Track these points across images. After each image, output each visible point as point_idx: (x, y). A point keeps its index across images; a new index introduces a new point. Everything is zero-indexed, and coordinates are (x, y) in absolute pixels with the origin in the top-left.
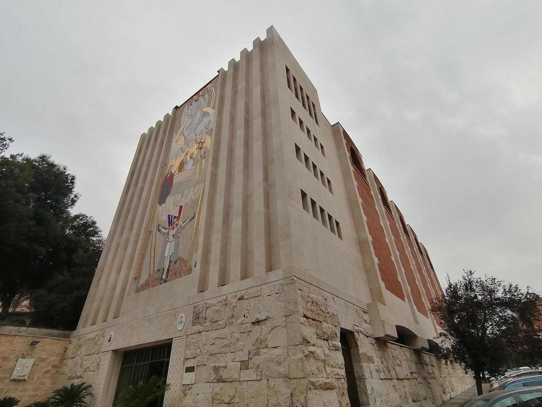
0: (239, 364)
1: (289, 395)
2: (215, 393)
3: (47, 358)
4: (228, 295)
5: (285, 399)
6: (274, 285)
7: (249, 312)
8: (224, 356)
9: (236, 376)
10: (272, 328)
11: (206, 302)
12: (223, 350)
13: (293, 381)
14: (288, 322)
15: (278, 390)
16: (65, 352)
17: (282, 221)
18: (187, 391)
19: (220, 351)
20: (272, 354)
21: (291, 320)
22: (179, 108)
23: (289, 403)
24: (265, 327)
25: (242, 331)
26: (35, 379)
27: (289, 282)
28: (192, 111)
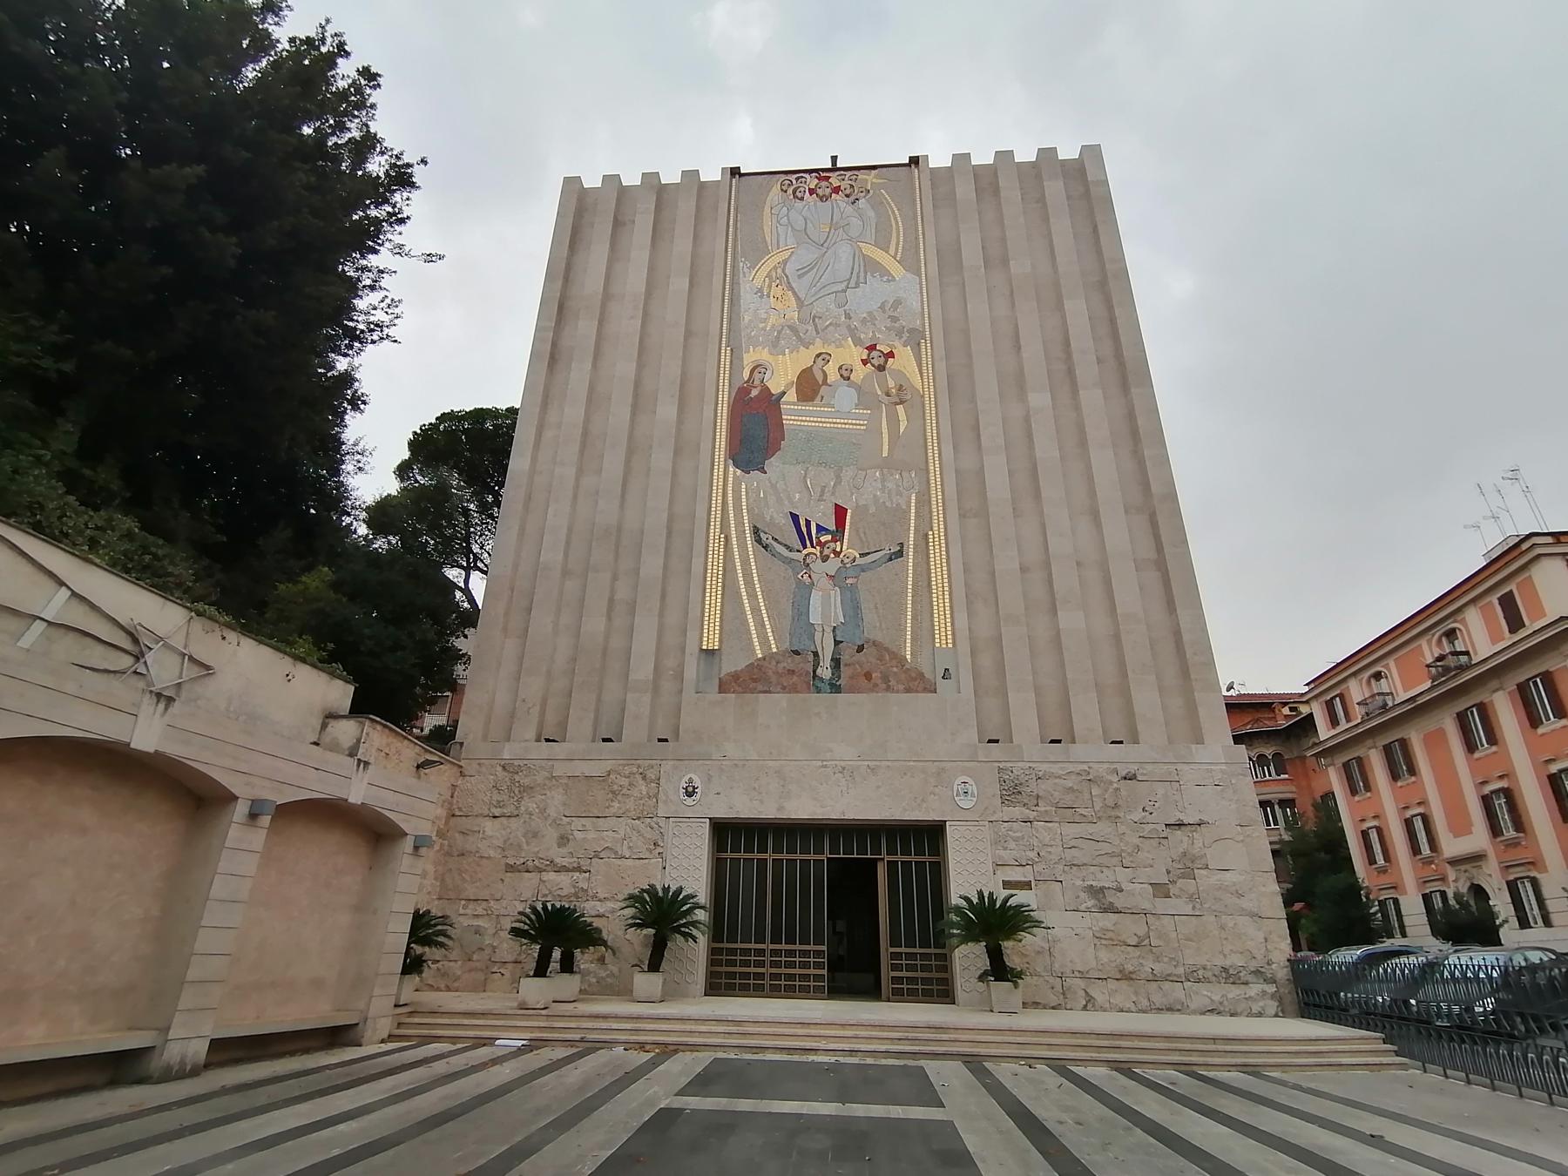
9: (1146, 905)
12: (1105, 860)
17: (1195, 654)
19: (1094, 863)
24: (1199, 837)
25: (485, 903)
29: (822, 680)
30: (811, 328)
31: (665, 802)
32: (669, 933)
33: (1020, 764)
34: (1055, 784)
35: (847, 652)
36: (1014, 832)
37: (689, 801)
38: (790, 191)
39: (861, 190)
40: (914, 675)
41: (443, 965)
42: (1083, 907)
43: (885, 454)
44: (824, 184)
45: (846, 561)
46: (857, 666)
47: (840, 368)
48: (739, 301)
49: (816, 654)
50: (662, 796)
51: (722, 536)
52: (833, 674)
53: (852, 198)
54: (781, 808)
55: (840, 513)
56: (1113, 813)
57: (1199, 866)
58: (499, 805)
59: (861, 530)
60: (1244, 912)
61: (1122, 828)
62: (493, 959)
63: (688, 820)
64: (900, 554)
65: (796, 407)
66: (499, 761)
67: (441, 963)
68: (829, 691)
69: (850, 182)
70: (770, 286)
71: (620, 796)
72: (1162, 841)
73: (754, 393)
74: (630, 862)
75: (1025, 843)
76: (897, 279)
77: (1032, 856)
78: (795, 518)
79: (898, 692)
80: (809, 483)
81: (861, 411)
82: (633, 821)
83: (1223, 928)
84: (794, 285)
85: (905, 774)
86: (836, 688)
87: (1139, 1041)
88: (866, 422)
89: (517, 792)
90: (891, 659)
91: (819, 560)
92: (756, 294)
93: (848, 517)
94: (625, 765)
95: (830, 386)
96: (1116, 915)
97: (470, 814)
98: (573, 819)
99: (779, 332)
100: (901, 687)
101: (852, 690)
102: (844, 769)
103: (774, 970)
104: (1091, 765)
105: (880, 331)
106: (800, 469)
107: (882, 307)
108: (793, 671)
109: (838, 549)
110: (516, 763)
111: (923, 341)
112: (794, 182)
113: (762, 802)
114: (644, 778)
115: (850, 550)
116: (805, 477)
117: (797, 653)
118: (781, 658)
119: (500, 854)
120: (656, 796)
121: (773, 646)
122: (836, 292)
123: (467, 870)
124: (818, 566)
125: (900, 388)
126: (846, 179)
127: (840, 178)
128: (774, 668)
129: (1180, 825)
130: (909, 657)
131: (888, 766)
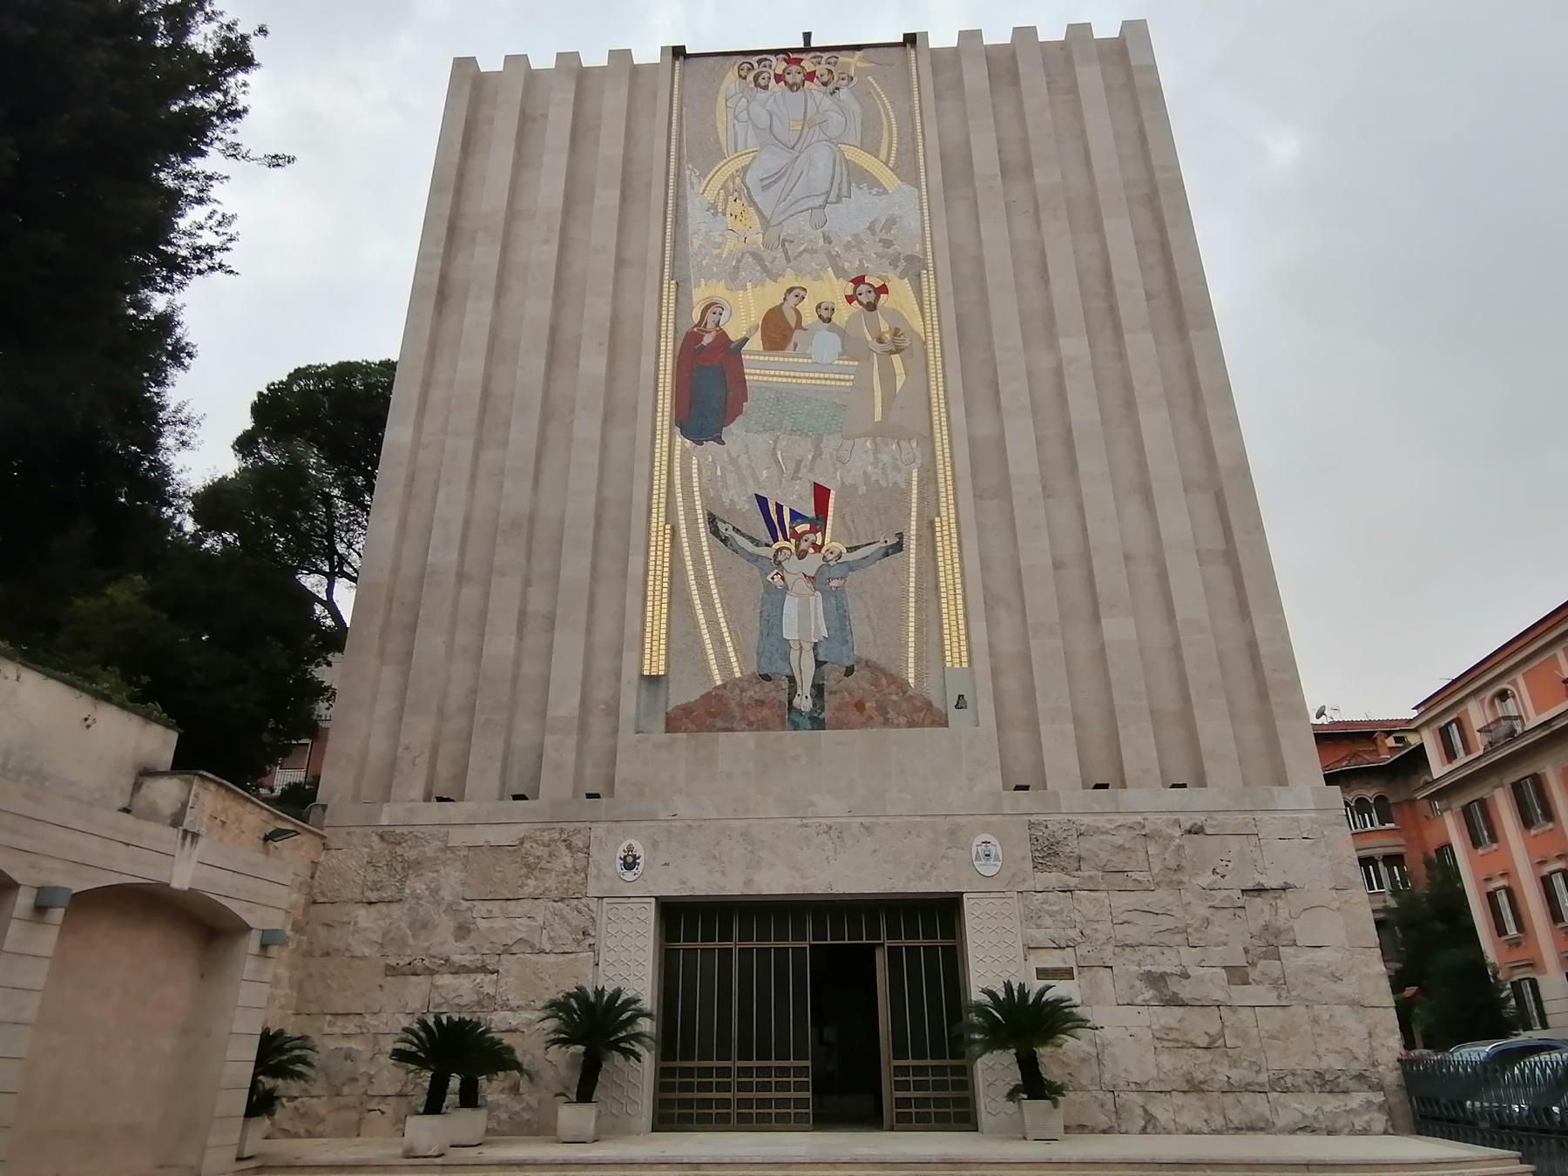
1: (1366, 1036)
2: (409, 928)
9: (1219, 995)
11: (1073, 818)
12: (1166, 938)
19: (1154, 941)
21: (1351, 898)
22: (687, 56)
23: (1367, 1048)
25: (1216, 903)
28: (774, 118)
29: (800, 712)
30: (779, 254)
31: (597, 878)
33: (1059, 817)
34: (1101, 841)
35: (831, 676)
36: (1051, 905)
37: (629, 876)
38: (750, 77)
39: (841, 76)
40: (919, 704)
41: (302, 1102)
42: (1139, 1000)
43: (878, 418)
44: (794, 68)
45: (830, 557)
47: (819, 306)
49: (792, 679)
50: (592, 870)
53: (831, 87)
54: (749, 882)
55: (821, 494)
57: (1285, 943)
59: (848, 518)
61: (1187, 896)
62: (369, 1093)
64: (899, 547)
65: (762, 358)
68: (810, 727)
70: (726, 201)
72: (1239, 912)
73: (707, 339)
74: (551, 958)
76: (890, 191)
78: (762, 502)
79: (898, 726)
81: (846, 363)
84: (757, 199)
86: (818, 723)
88: (852, 377)
90: (889, 684)
91: (795, 557)
92: (707, 211)
95: (806, 330)
97: (337, 900)
98: (475, 903)
100: (902, 720)
101: (840, 725)
102: (830, 828)
105: (869, 260)
106: (768, 438)
107: (871, 228)
109: (819, 542)
112: (756, 65)
114: (569, 847)
117: (767, 678)
120: (585, 869)
124: (792, 565)
125: (896, 333)
127: (814, 60)
129: (1260, 890)
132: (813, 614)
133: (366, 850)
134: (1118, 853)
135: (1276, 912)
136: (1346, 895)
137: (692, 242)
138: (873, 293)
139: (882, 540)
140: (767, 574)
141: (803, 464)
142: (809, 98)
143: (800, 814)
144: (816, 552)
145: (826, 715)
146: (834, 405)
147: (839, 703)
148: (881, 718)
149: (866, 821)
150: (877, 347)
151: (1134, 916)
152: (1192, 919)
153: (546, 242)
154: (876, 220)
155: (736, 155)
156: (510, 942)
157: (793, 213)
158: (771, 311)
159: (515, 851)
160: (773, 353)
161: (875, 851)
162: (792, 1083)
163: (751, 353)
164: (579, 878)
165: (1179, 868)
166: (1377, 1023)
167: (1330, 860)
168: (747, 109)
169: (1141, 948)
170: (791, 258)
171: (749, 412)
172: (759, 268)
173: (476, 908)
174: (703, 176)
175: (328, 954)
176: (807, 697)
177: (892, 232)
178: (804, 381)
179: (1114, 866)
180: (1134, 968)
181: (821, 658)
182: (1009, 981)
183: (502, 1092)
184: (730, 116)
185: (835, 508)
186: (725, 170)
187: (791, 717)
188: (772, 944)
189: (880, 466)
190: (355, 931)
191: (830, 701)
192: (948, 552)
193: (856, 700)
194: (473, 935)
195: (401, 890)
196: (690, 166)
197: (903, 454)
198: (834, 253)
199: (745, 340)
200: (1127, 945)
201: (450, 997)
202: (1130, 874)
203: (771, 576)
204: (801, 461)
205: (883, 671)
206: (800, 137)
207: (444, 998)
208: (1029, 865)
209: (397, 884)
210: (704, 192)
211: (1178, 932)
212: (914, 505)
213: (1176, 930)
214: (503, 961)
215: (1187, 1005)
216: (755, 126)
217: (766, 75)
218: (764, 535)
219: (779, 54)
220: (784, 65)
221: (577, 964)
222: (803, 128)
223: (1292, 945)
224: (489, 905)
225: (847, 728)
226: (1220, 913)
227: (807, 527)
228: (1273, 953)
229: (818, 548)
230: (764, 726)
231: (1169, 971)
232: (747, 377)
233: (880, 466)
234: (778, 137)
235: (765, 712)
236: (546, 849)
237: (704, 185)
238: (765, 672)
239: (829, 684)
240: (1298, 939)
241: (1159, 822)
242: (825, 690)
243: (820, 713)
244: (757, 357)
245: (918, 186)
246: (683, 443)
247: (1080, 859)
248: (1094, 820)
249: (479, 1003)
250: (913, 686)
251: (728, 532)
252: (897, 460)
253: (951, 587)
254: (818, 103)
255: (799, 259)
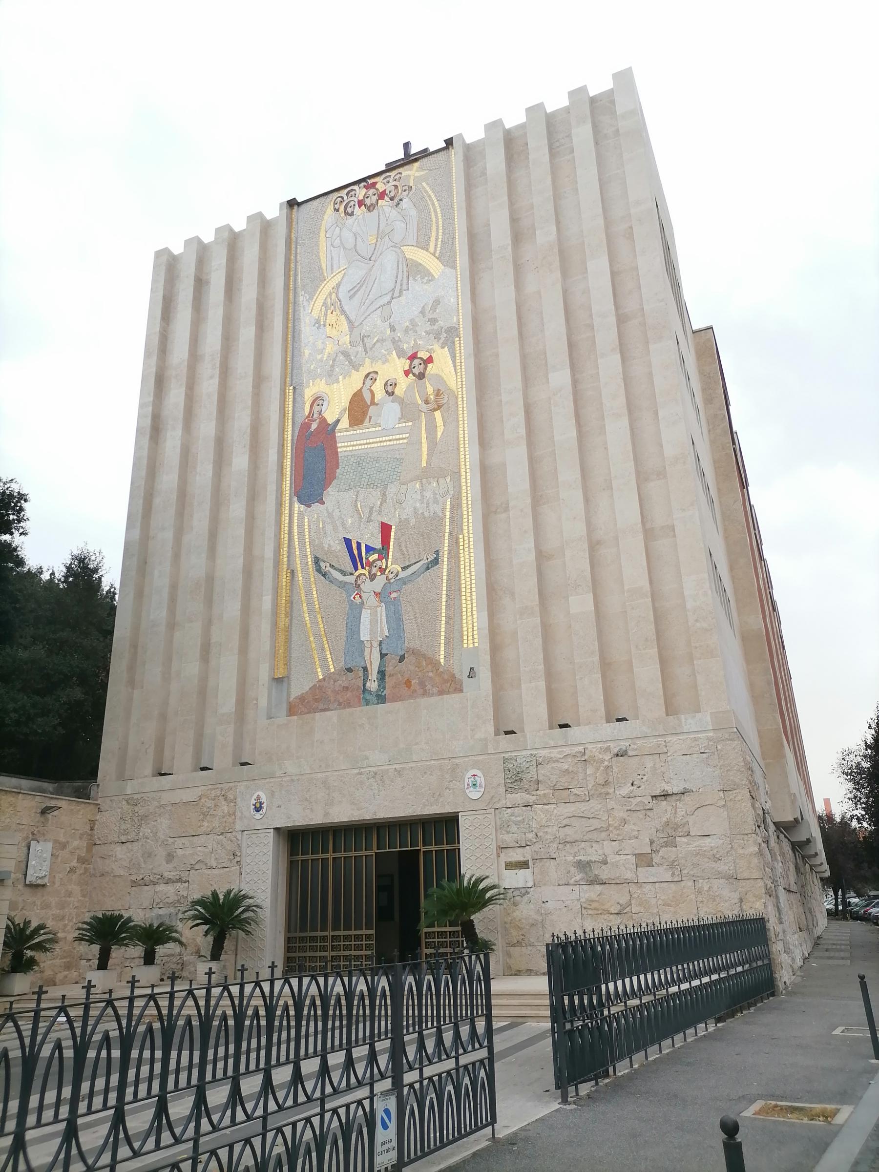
0: (633, 859)
1: (736, 901)
3: (68, 842)
4: (587, 746)
5: (731, 906)
6: (696, 739)
7: (642, 778)
8: (594, 845)
9: (629, 875)
10: (697, 806)
11: (534, 752)
12: (594, 836)
13: (742, 883)
14: (727, 799)
15: (717, 894)
16: (92, 829)
17: (697, 621)
18: (518, 898)
19: (585, 838)
20: (700, 846)
22: (299, 204)
24: (683, 807)
25: (633, 807)
26: (56, 886)
27: (727, 736)
28: (359, 239)
29: (370, 692)
30: (360, 349)
31: (241, 818)
32: (455, 885)
33: (524, 753)
34: (552, 768)
35: (390, 664)
36: (516, 817)
37: (258, 816)
38: (342, 209)
39: (404, 188)
40: (446, 677)
41: (93, 963)
42: (572, 882)
43: (424, 464)
44: (372, 191)
45: (391, 576)
46: (399, 675)
47: (386, 384)
48: (299, 335)
49: (365, 669)
50: (238, 814)
51: (289, 571)
52: (379, 686)
53: (396, 200)
54: (327, 814)
55: (385, 529)
56: (603, 790)
57: (681, 834)
58: (126, 832)
59: (403, 545)
60: (720, 875)
61: (611, 804)
62: (125, 956)
63: (257, 832)
64: (436, 561)
65: (348, 433)
66: (123, 797)
67: (92, 961)
68: (376, 702)
69: (394, 183)
70: (326, 315)
71: (208, 816)
72: (648, 813)
73: (314, 426)
74: (216, 871)
75: (525, 826)
76: (436, 277)
77: (530, 837)
78: (348, 542)
79: (433, 695)
80: (359, 506)
81: (404, 424)
82: (218, 837)
83: (699, 892)
84: (346, 308)
85: (425, 773)
86: (381, 699)
87: (539, 1014)
88: (408, 435)
89: (136, 821)
90: (427, 665)
91: (368, 580)
92: (314, 326)
93: (393, 534)
94: (212, 790)
95: (377, 404)
96: (603, 886)
97: (106, 842)
98: (175, 839)
99: (334, 360)
100: (435, 690)
101: (396, 699)
102: (376, 774)
103: (334, 953)
104: (587, 746)
105: (421, 338)
106: (352, 494)
107: (422, 312)
108: (347, 688)
109: (384, 567)
110: (135, 797)
111: (457, 339)
112: (345, 197)
113: (312, 810)
114: (225, 800)
115: (394, 566)
116: (356, 501)
117: (350, 670)
118: (337, 676)
119: (127, 872)
120: (234, 814)
121: (331, 667)
122: (382, 306)
123: (105, 887)
124: (368, 587)
125: (438, 393)
126: (391, 180)
127: (385, 181)
128: (332, 687)
129: (665, 796)
130: (442, 660)
131: (412, 768)
132: (379, 620)
133: (119, 810)
134: (564, 775)
135: (676, 811)
136: (731, 795)
137: (304, 352)
138: (423, 364)
139: (425, 558)
140: (351, 595)
141: (374, 509)
142: (381, 214)
143: (359, 765)
144: (382, 574)
145: (387, 692)
146: (395, 460)
147: (395, 683)
148: (422, 690)
149: (397, 766)
150: (424, 407)
151: (574, 822)
152: (614, 820)
153: (211, 377)
154: (426, 304)
155: (332, 276)
156: (194, 863)
157: (369, 313)
158: (355, 395)
159: (197, 805)
160: (356, 428)
161: (403, 787)
162: (353, 945)
163: (342, 431)
164: (230, 820)
165: (607, 783)
166: (747, 891)
167: (721, 769)
168: (340, 236)
169: (576, 844)
170: (368, 350)
171: (340, 476)
172: (347, 363)
173: (176, 843)
174: (311, 298)
175: (103, 875)
176: (374, 681)
177: (437, 311)
178: (376, 445)
179: (561, 785)
180: (570, 858)
181: (384, 652)
182: (215, 890)
183: (192, 954)
184: (329, 244)
185: (395, 539)
186: (327, 288)
187: (365, 697)
188: (353, 854)
189: (425, 501)
190: (116, 861)
191: (389, 682)
192: (467, 560)
193: (406, 679)
194: (175, 860)
195: (138, 834)
196: (303, 293)
197: (441, 488)
198: (397, 339)
199: (338, 421)
200: (568, 842)
201: (163, 898)
202: (572, 790)
203: (353, 596)
204: (373, 507)
205: (424, 656)
206: (375, 249)
207: (160, 899)
208: (502, 789)
209: (136, 830)
210: (312, 311)
211: (603, 831)
212: (447, 527)
213: (602, 829)
214: (191, 875)
215: (605, 883)
216: (344, 248)
217: (352, 203)
218: (349, 567)
219: (360, 183)
220: (364, 190)
221: (230, 874)
222: (377, 241)
223: (688, 835)
224: (183, 840)
225: (400, 701)
226: (635, 814)
227: (376, 556)
228: (671, 842)
229: (382, 571)
230: (348, 705)
231: (593, 859)
232: (339, 450)
233: (425, 501)
234: (360, 252)
235: (349, 694)
236: (213, 802)
237: (312, 306)
238: (349, 666)
239: (389, 670)
240: (691, 830)
241: (594, 750)
242: (386, 674)
243: (383, 692)
244: (345, 433)
245: (454, 267)
246: (299, 508)
247: (538, 782)
248: (550, 753)
249: (178, 901)
250: (442, 664)
251: (327, 569)
252: (436, 494)
253: (469, 587)
254: (387, 216)
255: (373, 349)
